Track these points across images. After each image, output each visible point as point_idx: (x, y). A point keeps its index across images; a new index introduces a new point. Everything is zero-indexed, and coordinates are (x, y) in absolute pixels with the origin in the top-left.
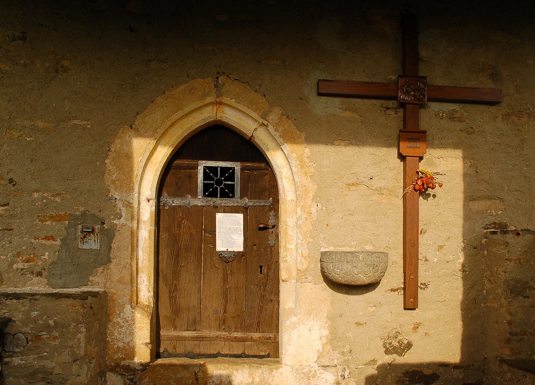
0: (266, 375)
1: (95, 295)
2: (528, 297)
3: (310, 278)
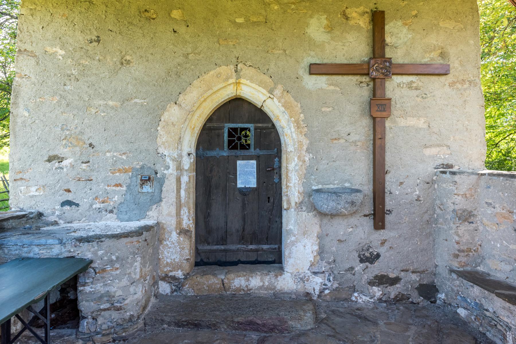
0: (273, 280)
1: (148, 228)
2: (472, 223)
3: (304, 208)
